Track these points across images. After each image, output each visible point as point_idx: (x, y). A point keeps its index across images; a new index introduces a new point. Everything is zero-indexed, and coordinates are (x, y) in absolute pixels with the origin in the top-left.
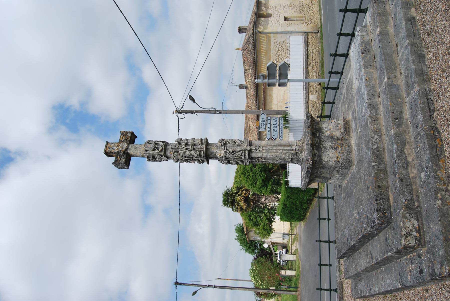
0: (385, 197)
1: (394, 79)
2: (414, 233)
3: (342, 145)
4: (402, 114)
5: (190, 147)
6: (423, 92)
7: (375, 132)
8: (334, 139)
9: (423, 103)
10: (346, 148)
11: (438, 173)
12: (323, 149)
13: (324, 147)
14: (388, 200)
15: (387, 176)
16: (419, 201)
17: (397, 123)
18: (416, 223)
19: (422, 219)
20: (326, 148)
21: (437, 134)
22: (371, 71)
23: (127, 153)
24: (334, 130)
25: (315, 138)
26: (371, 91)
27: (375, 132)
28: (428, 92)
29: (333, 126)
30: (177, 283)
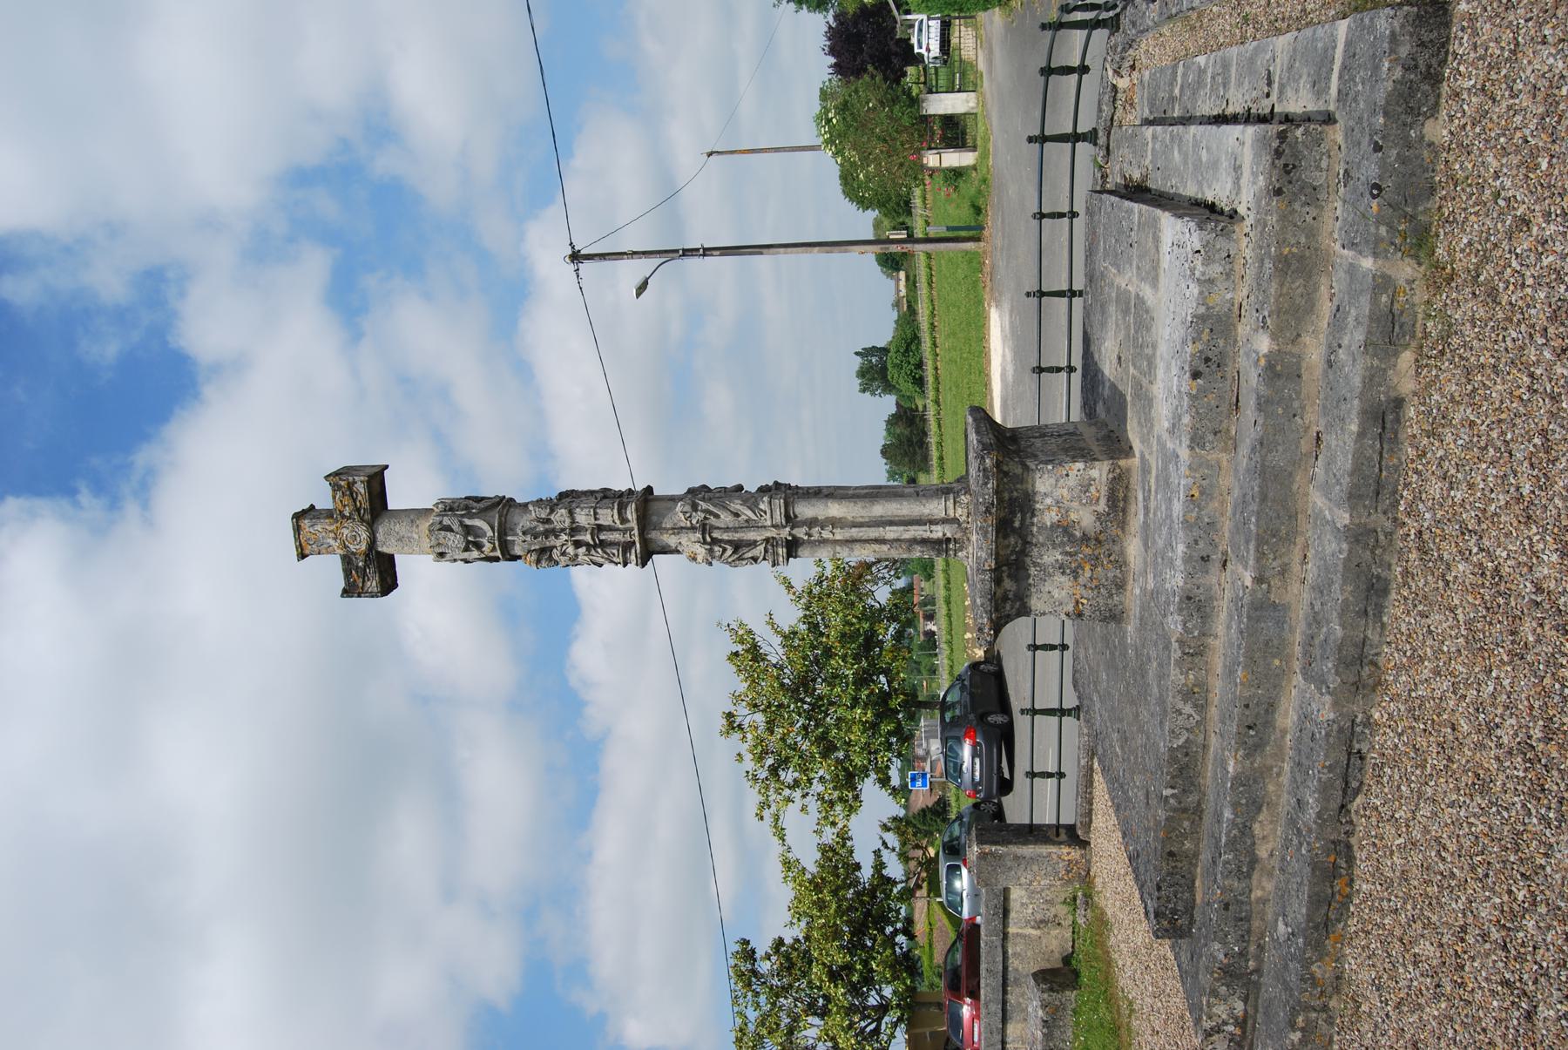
0: (1182, 881)
1: (1275, 582)
2: (1230, 1028)
3: (1095, 561)
4: (1273, 712)
5: (588, 538)
6: (1341, 730)
7: (1188, 694)
8: (1071, 536)
9: (1331, 769)
10: (1107, 573)
11: (1314, 968)
12: (1033, 571)
13: (1035, 564)
14: (1191, 888)
15: (1199, 825)
16: (1259, 959)
17: (1250, 742)
18: (1239, 1006)
19: (1256, 999)
20: (1043, 568)
21: (1344, 865)
22: (1213, 456)
23: (379, 553)
24: (1075, 504)
25: (1006, 537)
26: (1201, 545)
27: (1188, 694)
28: (1358, 729)
29: (1071, 489)
30: (576, 257)
